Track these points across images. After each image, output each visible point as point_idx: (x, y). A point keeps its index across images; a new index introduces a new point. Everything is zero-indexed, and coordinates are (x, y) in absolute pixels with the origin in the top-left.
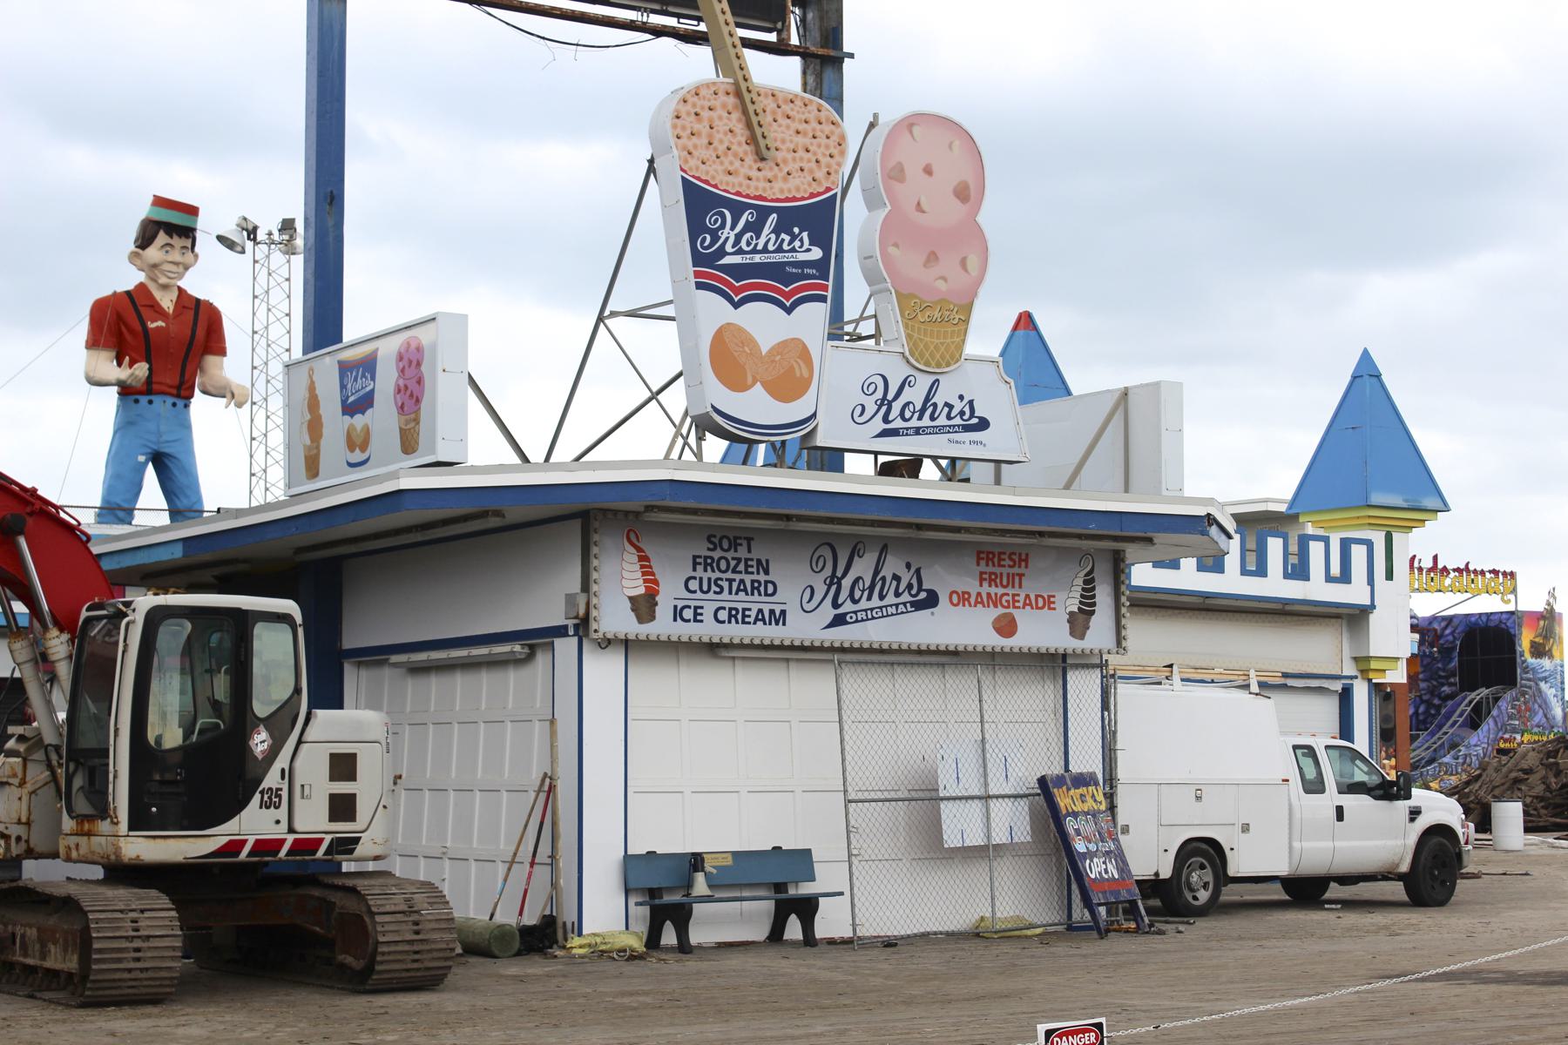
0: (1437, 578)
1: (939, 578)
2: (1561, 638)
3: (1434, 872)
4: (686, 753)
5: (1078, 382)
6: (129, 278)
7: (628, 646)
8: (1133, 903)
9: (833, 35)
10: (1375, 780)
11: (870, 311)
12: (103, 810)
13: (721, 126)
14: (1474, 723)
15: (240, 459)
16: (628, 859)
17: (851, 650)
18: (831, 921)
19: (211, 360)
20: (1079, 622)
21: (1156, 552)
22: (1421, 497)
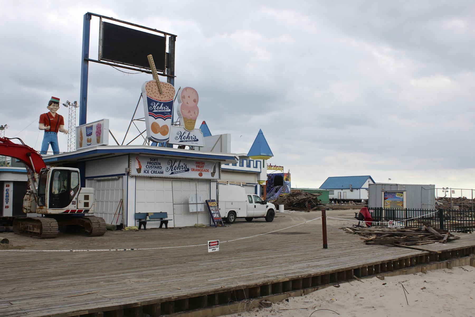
1: (190, 166)
3: (270, 216)
4: (145, 196)
5: (213, 133)
6: (47, 111)
7: (136, 177)
8: (221, 222)
9: (173, 73)
10: (261, 201)
11: (178, 120)
12: (44, 205)
13: (154, 88)
14: (276, 192)
15: (67, 143)
16: (136, 214)
17: (174, 178)
18: (170, 225)
19: (61, 126)
20: (213, 174)
21: (226, 163)
22: (269, 154)
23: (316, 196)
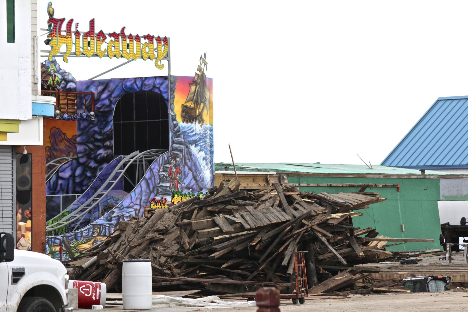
0: (93, 43)
2: (211, 103)
14: (127, 186)
23: (344, 208)
